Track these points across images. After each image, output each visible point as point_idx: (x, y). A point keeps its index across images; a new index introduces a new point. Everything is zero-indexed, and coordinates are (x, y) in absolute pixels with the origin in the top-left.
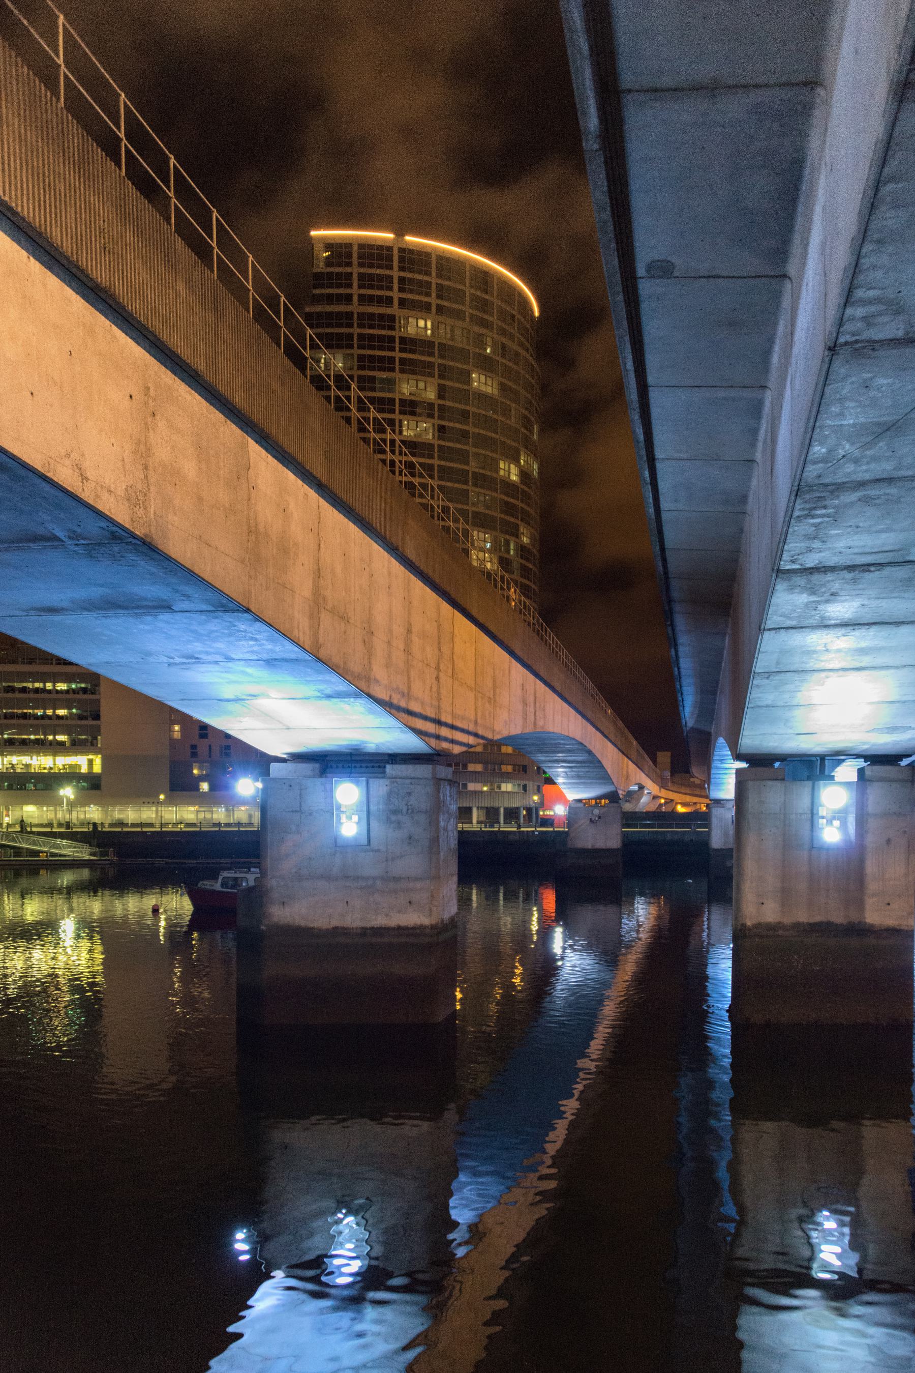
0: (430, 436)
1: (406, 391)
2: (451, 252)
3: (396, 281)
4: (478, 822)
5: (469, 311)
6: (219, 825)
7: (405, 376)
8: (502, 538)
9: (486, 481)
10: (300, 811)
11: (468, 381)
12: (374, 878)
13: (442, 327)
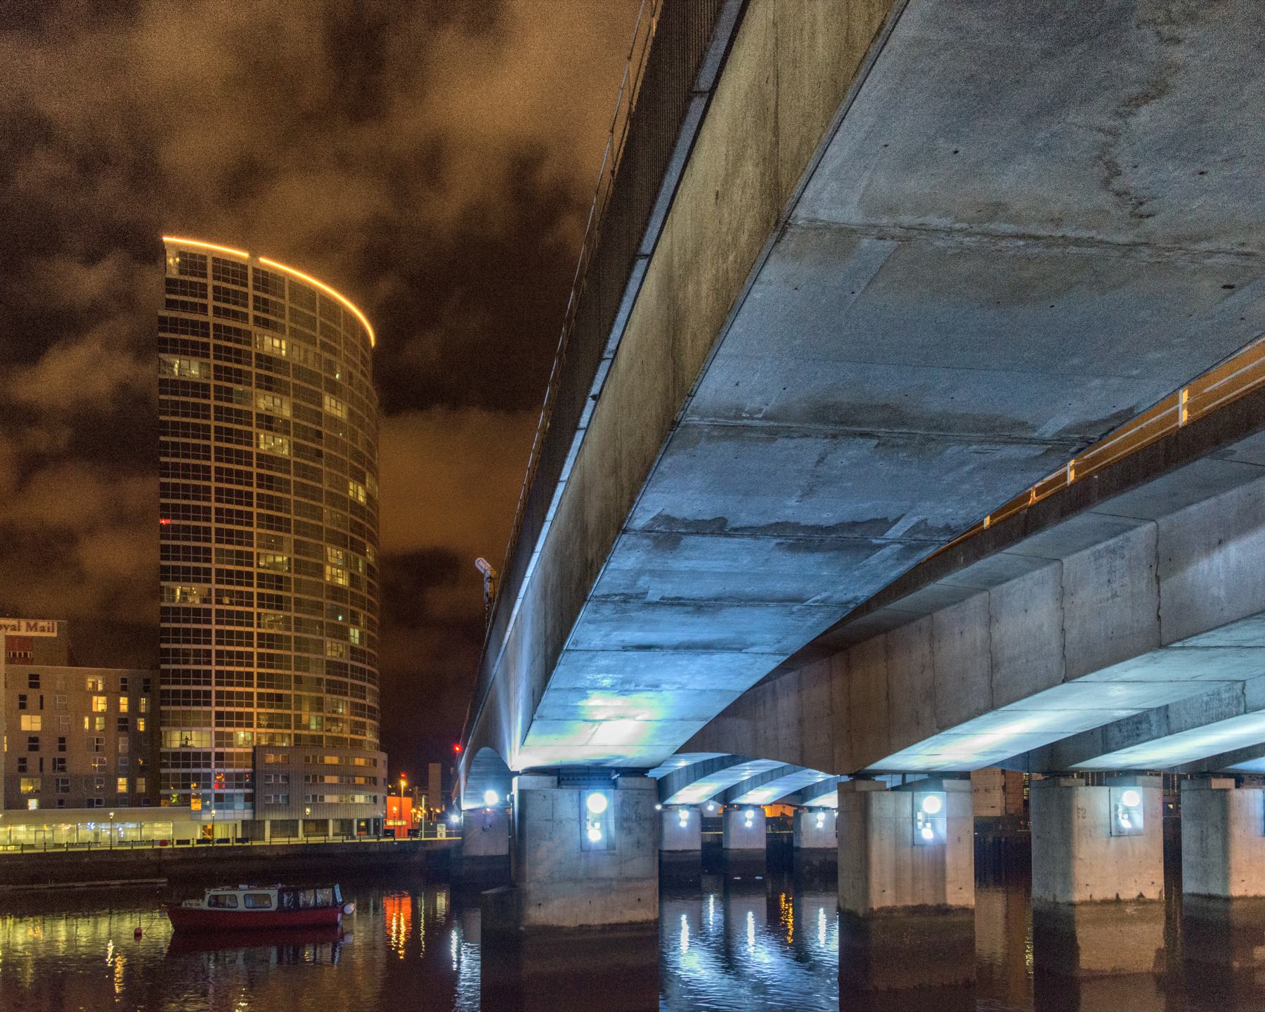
0: (286, 452)
1: (262, 406)
2: (305, 281)
3: (210, 289)
4: (335, 835)
5: (319, 338)
6: (60, 846)
7: (263, 391)
8: (352, 554)
9: (339, 500)
10: (552, 820)
11: (321, 404)
12: (611, 879)
13: (296, 349)
